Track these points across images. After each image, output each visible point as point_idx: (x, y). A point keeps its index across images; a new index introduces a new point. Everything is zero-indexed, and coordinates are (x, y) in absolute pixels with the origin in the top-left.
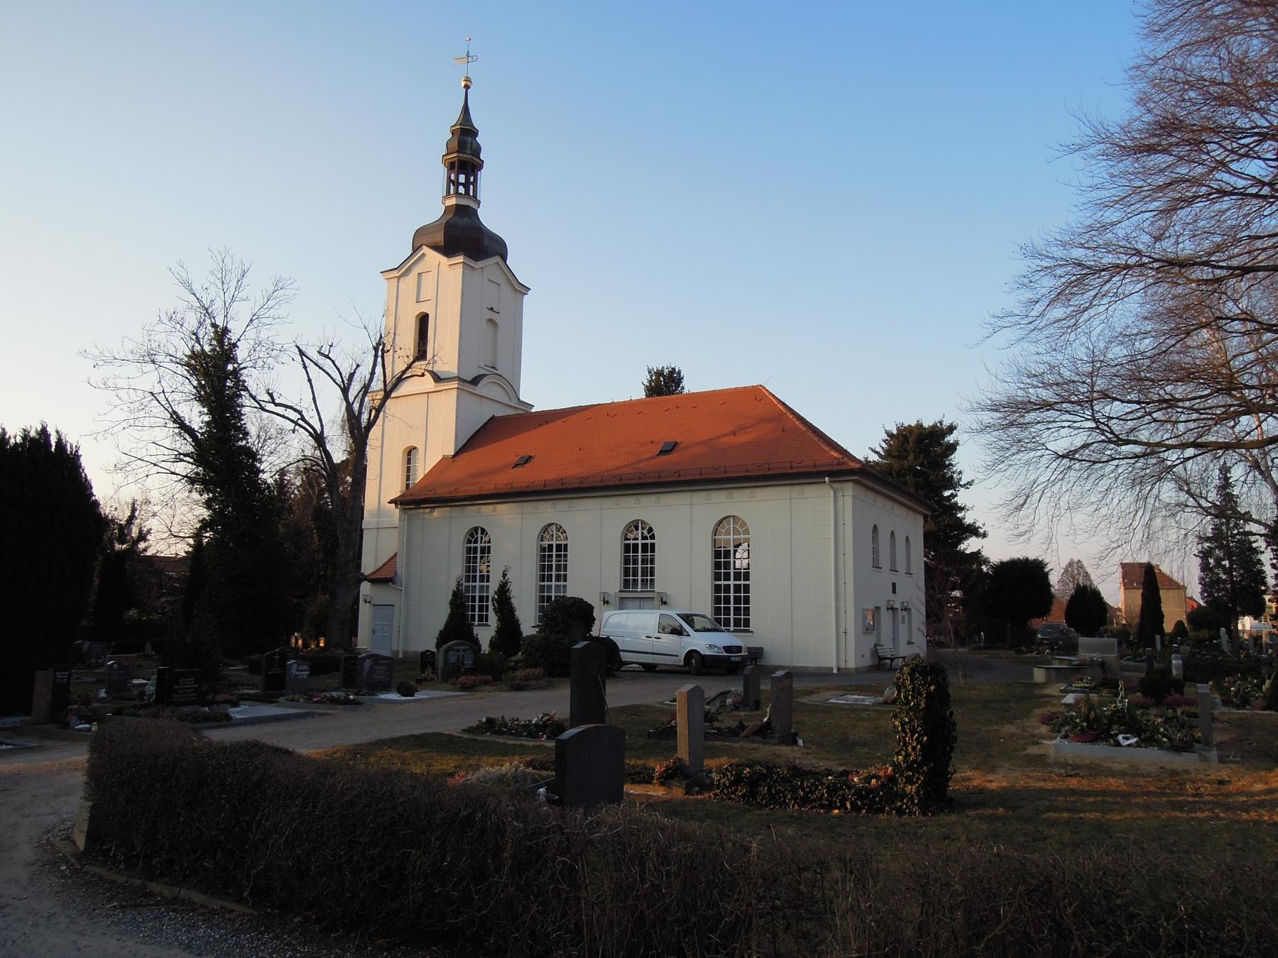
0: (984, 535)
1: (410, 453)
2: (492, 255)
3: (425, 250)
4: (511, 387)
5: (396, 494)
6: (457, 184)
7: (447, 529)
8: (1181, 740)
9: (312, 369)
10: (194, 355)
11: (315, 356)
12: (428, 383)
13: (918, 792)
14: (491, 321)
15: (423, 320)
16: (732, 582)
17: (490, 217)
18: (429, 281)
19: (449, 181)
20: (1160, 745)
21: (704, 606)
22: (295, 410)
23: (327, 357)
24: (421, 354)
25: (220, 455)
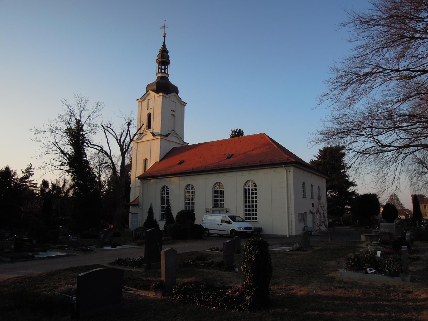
0: (356, 185)
1: (146, 160)
2: (172, 92)
3: (150, 91)
4: (181, 138)
5: (138, 175)
6: (162, 69)
7: (156, 186)
8: (395, 271)
9: (107, 132)
10: (68, 129)
11: (106, 128)
12: (151, 137)
13: (250, 299)
14: (173, 115)
15: (150, 115)
16: (251, 204)
17: (172, 80)
18: (151, 102)
19: (159, 68)
20: (385, 274)
21: (241, 213)
22: (99, 147)
23: (110, 128)
24: (149, 127)
25: (77, 162)
